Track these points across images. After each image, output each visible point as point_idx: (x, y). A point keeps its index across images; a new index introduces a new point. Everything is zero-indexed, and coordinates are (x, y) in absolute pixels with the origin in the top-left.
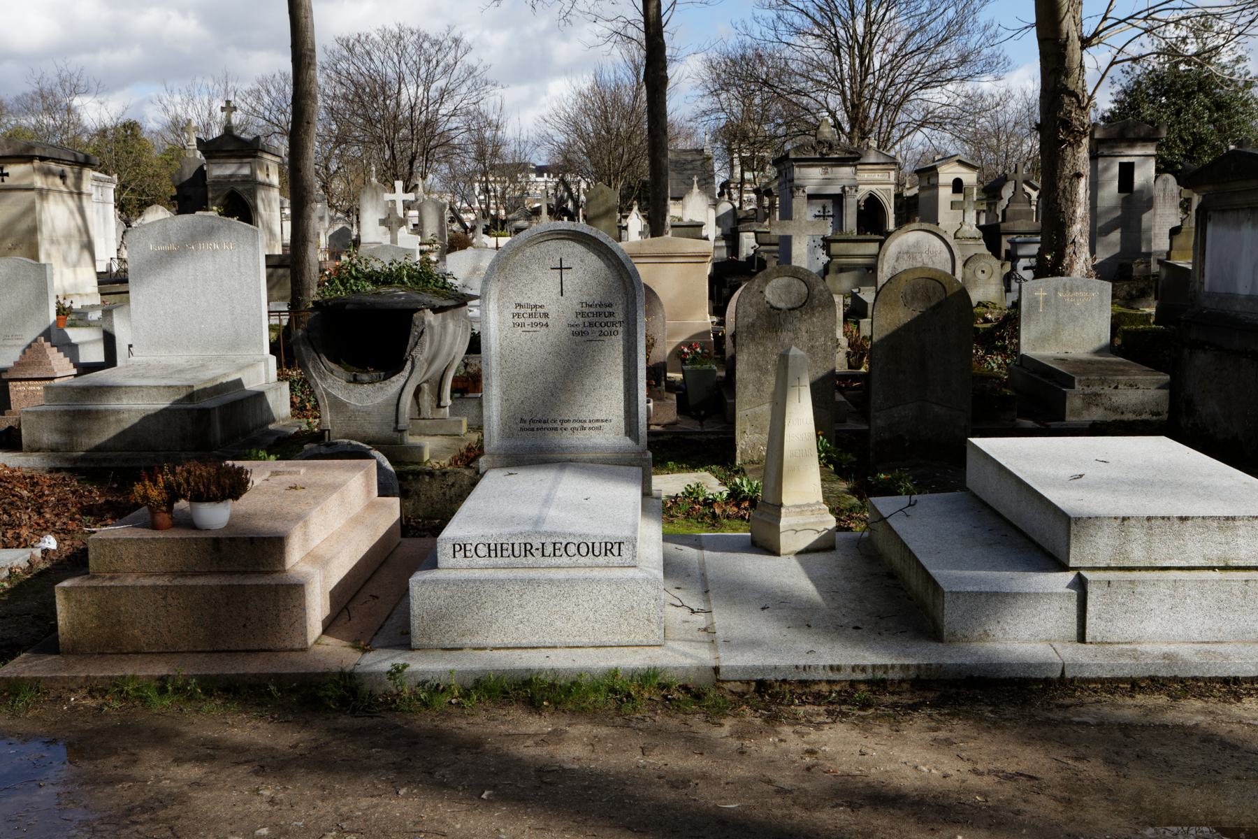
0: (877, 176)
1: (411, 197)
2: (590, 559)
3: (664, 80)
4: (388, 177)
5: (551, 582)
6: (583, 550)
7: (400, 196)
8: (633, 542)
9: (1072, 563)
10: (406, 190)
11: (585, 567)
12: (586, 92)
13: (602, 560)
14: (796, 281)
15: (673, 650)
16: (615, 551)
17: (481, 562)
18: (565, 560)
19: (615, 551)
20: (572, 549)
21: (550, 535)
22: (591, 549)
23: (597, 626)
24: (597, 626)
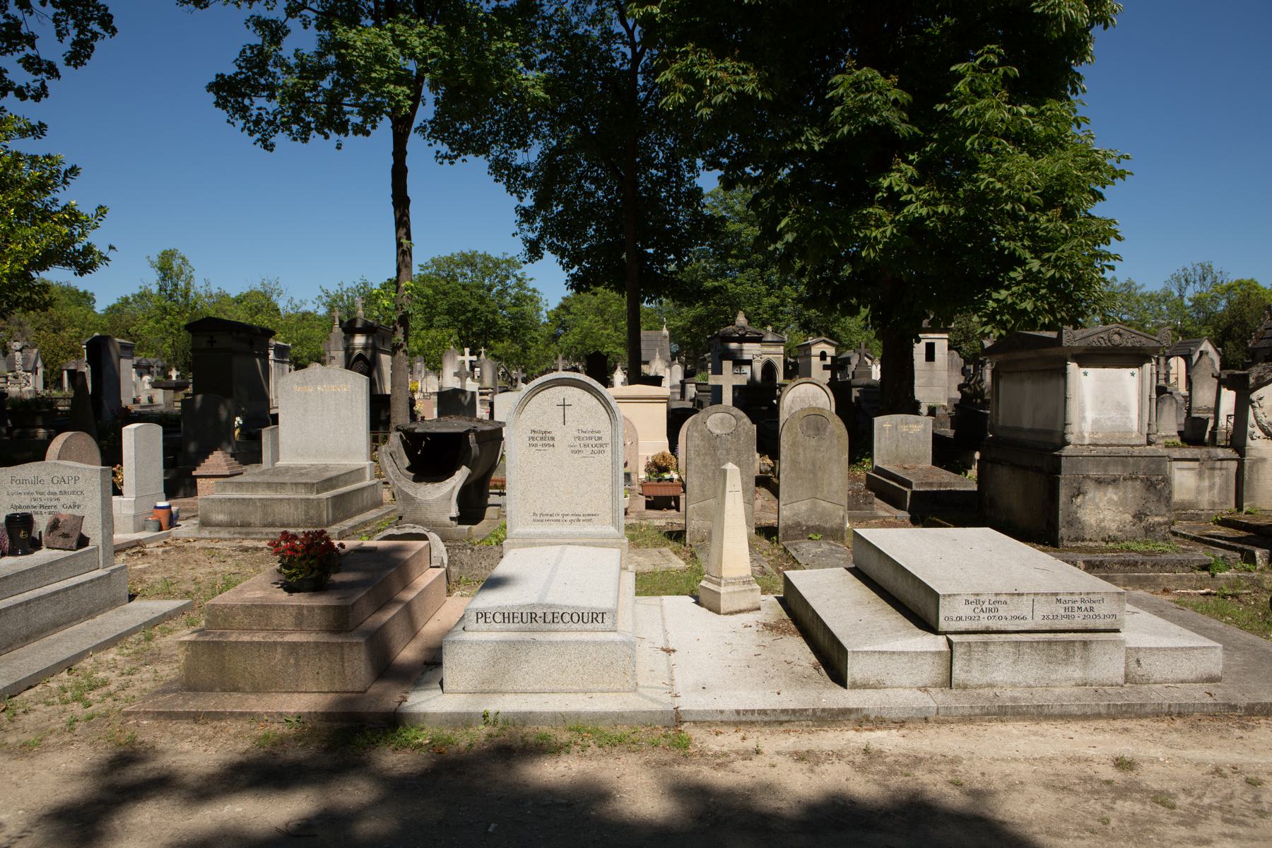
0: (773, 349)
1: (474, 358)
2: (580, 625)
3: (405, 170)
4: (461, 346)
5: (550, 643)
6: (575, 618)
7: (467, 358)
8: (614, 613)
9: (943, 625)
10: (471, 354)
11: (577, 631)
12: (192, 294)
13: (589, 626)
15: (644, 697)
16: (600, 619)
17: (498, 626)
18: (561, 625)
19: (600, 619)
20: (566, 618)
21: (550, 606)
22: (581, 618)
23: (585, 677)
24: (585, 677)
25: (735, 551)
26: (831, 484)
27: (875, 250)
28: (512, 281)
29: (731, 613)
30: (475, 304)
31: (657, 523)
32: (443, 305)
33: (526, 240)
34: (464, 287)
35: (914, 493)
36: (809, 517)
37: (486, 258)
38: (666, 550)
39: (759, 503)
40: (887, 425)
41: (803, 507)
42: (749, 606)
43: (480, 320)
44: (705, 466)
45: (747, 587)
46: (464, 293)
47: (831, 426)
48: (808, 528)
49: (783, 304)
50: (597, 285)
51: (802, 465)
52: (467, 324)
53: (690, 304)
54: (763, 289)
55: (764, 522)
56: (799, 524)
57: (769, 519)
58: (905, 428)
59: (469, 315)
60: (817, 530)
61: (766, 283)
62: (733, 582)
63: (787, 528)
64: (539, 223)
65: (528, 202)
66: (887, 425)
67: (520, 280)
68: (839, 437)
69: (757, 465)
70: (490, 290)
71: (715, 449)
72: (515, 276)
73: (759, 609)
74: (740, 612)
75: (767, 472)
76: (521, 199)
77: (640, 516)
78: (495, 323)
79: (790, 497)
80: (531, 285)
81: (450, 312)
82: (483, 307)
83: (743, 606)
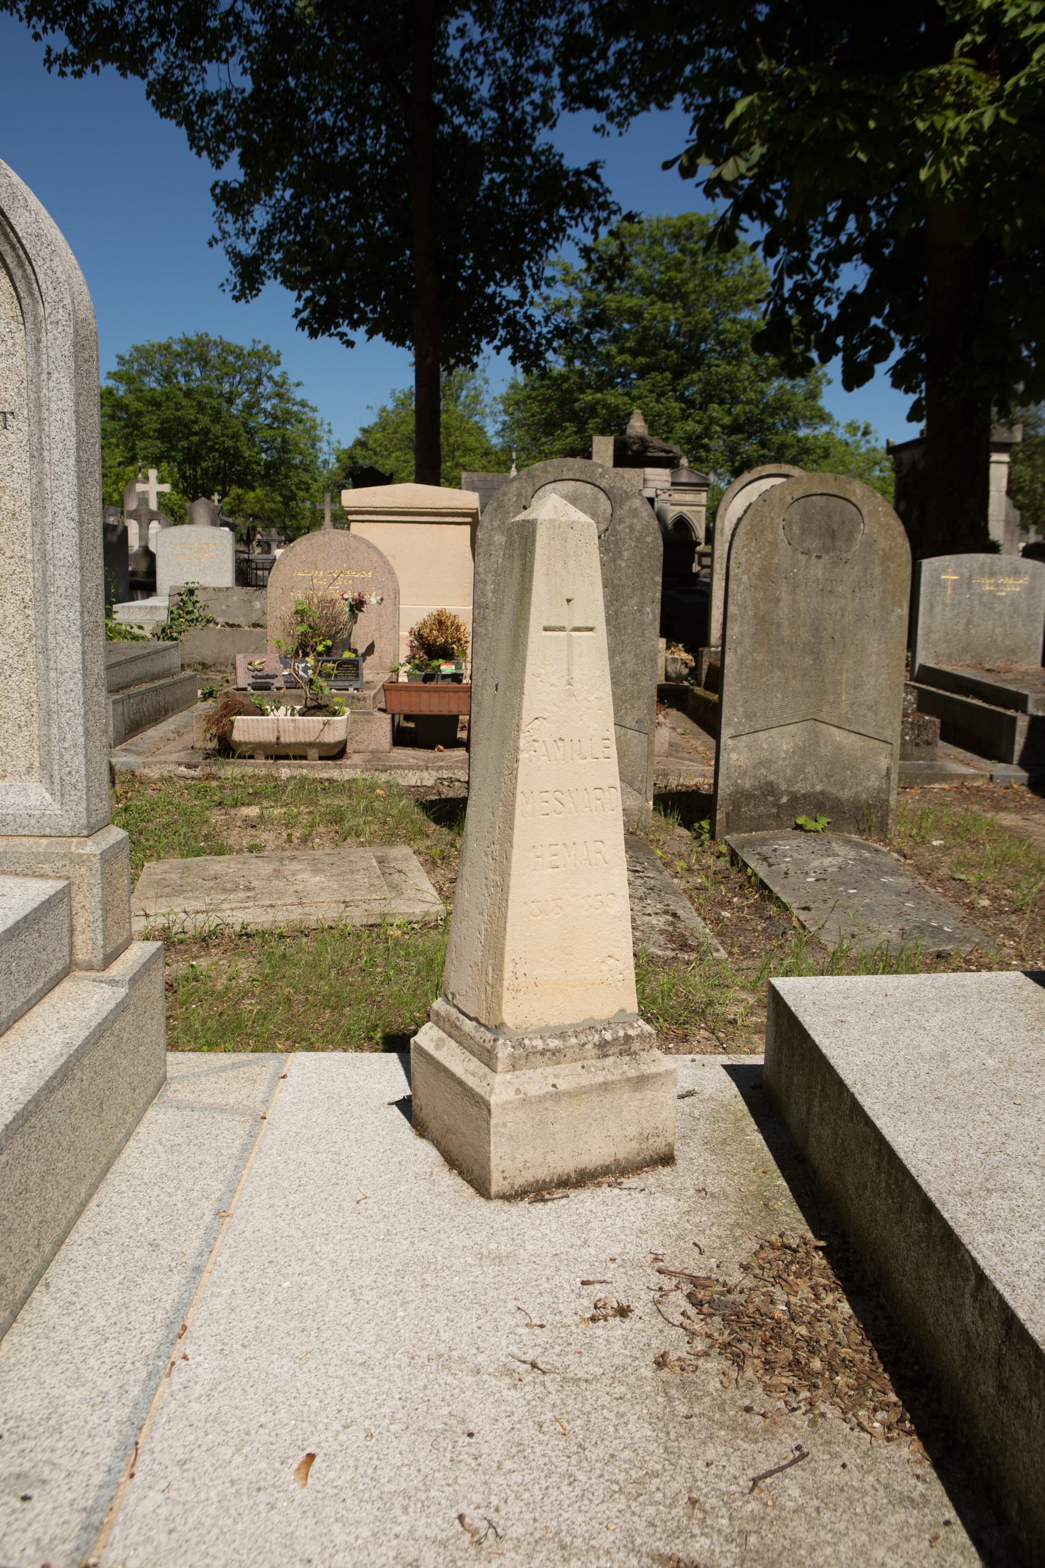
0: (688, 497)
14: (588, 488)
25: (566, 892)
26: (858, 685)
27: (950, 166)
28: (267, 388)
29: (538, 1192)
30: (205, 420)
31: (412, 779)
32: (151, 422)
33: (236, 257)
34: (188, 394)
35: (1034, 721)
36: (799, 769)
37: (227, 349)
38: (402, 853)
39: (663, 735)
40: (949, 577)
41: (782, 743)
43: (212, 449)
45: (617, 1067)
46: (185, 402)
47: (865, 529)
48: (794, 799)
49: (707, 433)
50: (354, 325)
51: (785, 632)
52: (193, 457)
54: (676, 407)
55: (674, 783)
56: (769, 789)
57: (693, 775)
58: (987, 585)
59: (195, 439)
60: (818, 804)
61: (681, 398)
62: (552, 1048)
63: (740, 797)
64: (260, 217)
65: (233, 172)
66: (949, 577)
68: (886, 558)
69: (661, 662)
70: (230, 401)
73: (667, 1159)
75: (680, 677)
76: (218, 164)
77: (376, 762)
78: (238, 455)
79: (750, 716)
80: (298, 394)
81: (163, 434)
82: (217, 429)
83: (597, 1152)
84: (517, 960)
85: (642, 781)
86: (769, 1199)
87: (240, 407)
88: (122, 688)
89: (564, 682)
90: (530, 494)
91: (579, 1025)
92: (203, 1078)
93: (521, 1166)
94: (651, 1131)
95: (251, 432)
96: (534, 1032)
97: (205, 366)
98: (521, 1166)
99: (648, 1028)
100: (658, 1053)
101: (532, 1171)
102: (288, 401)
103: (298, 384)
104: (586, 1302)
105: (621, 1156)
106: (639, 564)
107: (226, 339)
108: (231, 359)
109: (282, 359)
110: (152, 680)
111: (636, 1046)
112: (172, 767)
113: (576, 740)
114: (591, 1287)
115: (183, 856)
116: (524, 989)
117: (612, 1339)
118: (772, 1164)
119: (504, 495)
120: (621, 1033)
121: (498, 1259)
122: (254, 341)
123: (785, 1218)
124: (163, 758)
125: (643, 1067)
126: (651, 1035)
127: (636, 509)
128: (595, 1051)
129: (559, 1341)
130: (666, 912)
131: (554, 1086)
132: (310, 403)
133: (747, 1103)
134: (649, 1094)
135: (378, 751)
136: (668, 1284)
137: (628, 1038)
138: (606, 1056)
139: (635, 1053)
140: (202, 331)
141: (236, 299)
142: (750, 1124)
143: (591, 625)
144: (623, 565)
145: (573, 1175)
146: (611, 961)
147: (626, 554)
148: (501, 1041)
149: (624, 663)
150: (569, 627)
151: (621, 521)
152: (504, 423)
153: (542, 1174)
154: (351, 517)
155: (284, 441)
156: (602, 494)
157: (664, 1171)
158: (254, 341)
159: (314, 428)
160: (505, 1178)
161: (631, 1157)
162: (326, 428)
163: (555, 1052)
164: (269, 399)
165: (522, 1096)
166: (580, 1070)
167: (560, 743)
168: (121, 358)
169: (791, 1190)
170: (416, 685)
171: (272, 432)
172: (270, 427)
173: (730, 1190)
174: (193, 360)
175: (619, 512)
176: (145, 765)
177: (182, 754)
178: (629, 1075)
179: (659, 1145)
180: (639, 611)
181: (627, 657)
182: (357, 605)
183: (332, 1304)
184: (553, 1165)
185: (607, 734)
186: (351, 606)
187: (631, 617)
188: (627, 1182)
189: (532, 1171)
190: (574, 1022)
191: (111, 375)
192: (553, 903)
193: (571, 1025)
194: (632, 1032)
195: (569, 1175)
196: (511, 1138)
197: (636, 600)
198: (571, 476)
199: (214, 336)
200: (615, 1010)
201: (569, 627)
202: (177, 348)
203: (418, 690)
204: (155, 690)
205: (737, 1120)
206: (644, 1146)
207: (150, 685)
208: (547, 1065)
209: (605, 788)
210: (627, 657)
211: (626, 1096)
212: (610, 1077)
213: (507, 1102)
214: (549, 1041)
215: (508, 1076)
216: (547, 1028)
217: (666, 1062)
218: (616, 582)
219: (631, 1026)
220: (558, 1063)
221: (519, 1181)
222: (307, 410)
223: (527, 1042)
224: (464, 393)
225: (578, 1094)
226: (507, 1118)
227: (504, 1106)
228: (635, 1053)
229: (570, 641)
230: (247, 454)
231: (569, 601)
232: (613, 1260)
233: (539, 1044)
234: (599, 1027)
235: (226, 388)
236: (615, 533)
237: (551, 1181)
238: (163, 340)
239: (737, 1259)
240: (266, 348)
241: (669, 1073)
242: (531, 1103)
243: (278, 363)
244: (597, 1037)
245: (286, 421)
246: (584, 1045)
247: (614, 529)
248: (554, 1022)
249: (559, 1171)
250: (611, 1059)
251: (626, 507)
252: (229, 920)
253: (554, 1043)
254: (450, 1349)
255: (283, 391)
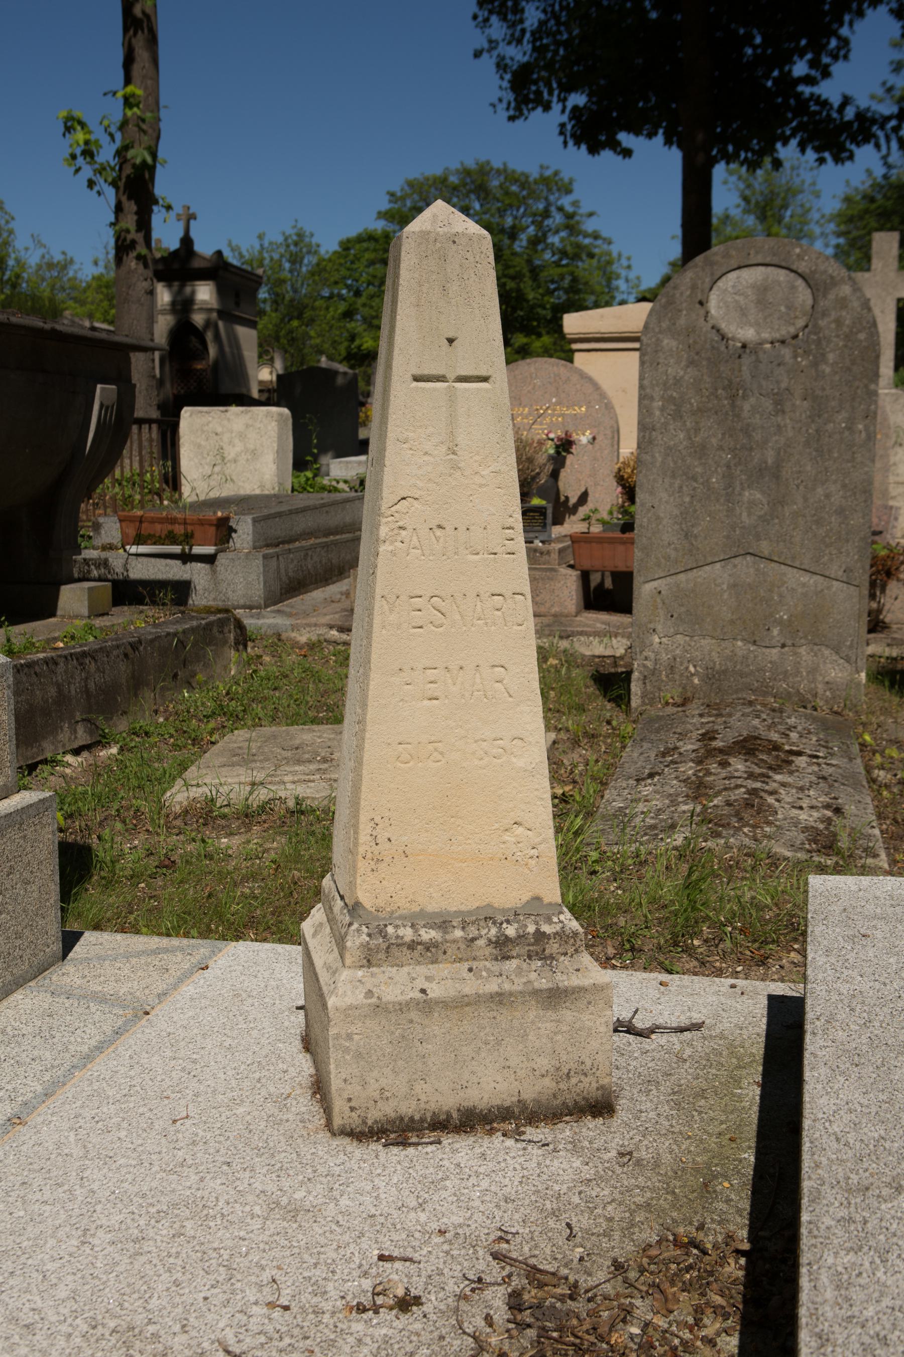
14: (782, 275)
28: (557, 219)
29: (399, 1132)
33: (502, 66)
37: (510, 177)
42: (532, 1090)
44: (701, 451)
45: (521, 975)
53: (841, 155)
67: (570, 216)
71: (734, 391)
72: (560, 209)
73: (601, 1107)
74: (469, 1121)
80: (589, 226)
83: (490, 1086)
84: (377, 819)
85: (851, 647)
86: (715, 1177)
87: (524, 243)
88: (283, 543)
89: (444, 449)
90: (707, 286)
91: (470, 913)
92: (107, 963)
93: (376, 1095)
94: (573, 1066)
95: (535, 272)
96: (403, 917)
97: (485, 199)
98: (376, 1095)
99: (575, 925)
100: (586, 958)
101: (393, 1103)
102: (579, 233)
103: (591, 215)
104: (367, 1284)
105: (528, 1095)
106: (849, 369)
107: (511, 166)
108: (514, 188)
109: (576, 186)
110: (326, 535)
111: (553, 947)
112: (322, 631)
113: (461, 528)
114: (388, 1265)
115: (287, 725)
116: (388, 859)
117: (368, 1340)
118: (751, 1130)
119: (675, 288)
120: (531, 929)
121: (294, 1212)
122: (542, 167)
123: (722, 1206)
124: (313, 620)
125: (559, 977)
126: (575, 934)
127: (844, 299)
128: (489, 950)
129: (296, 1331)
130: (827, 806)
131: (423, 991)
132: (604, 234)
133: (767, 1047)
134: (568, 1015)
135: (562, 615)
136: (495, 1272)
137: (540, 936)
138: (507, 958)
139: (552, 958)
140: (483, 159)
141: (512, 119)
142: (756, 1073)
143: (484, 373)
144: (828, 370)
145: (455, 1115)
146: (520, 830)
147: (831, 357)
148: (355, 926)
149: (828, 496)
150: (451, 376)
151: (824, 314)
152: (837, 246)
153: (408, 1109)
154: (575, 346)
155: (575, 280)
156: (800, 282)
157: (591, 1126)
158: (542, 167)
159: (609, 263)
160: (352, 1109)
161: (544, 1098)
162: (624, 262)
163: (429, 946)
164: (557, 232)
165: (374, 1000)
166: (466, 974)
167: (439, 532)
168: (392, 194)
169: (756, 1169)
170: (611, 535)
171: (559, 270)
172: (557, 264)
173: (667, 1158)
174: (470, 191)
175: (822, 303)
176: (294, 628)
177: (337, 616)
178: (537, 985)
179: (588, 1086)
180: (849, 428)
181: (833, 488)
182: (565, 445)
183: (51, 1242)
184: (423, 1098)
185: (510, 522)
186: (557, 447)
187: (837, 436)
188: (531, 1132)
189: (393, 1103)
190: (463, 908)
191: (381, 215)
192: (431, 747)
193: (458, 913)
194: (546, 928)
195: (449, 1115)
196: (359, 1056)
197: (844, 415)
198: (759, 259)
199: (497, 164)
200: (526, 897)
201: (451, 376)
202: (454, 179)
203: (612, 541)
204: (326, 546)
205: (739, 1067)
206: (562, 1086)
207: (325, 540)
208: (419, 963)
209: (508, 594)
210: (833, 488)
211: (532, 1015)
212: (507, 986)
213: (351, 1007)
214: (422, 932)
215: (360, 973)
216: (422, 914)
217: (588, 972)
218: (818, 392)
219: (549, 920)
220: (435, 961)
221: (374, 1115)
222: (599, 242)
223: (390, 930)
224: (788, 213)
225: (458, 1004)
226: (353, 1029)
227: (348, 1011)
228: (552, 958)
229: (452, 397)
230: (531, 296)
231: (451, 341)
232: (442, 1232)
233: (407, 934)
234: (500, 918)
235: (509, 221)
236: (817, 330)
237: (422, 1120)
238: (438, 172)
239: (617, 1252)
240: (556, 173)
241: (599, 988)
242: (387, 1010)
243: (569, 191)
244: (494, 931)
245: (576, 257)
246: (473, 940)
247: (815, 325)
248: (432, 907)
249: (432, 1106)
250: (514, 963)
251: (831, 296)
252: (282, 794)
253: (427, 935)
254: (150, 1322)
255: (572, 222)
